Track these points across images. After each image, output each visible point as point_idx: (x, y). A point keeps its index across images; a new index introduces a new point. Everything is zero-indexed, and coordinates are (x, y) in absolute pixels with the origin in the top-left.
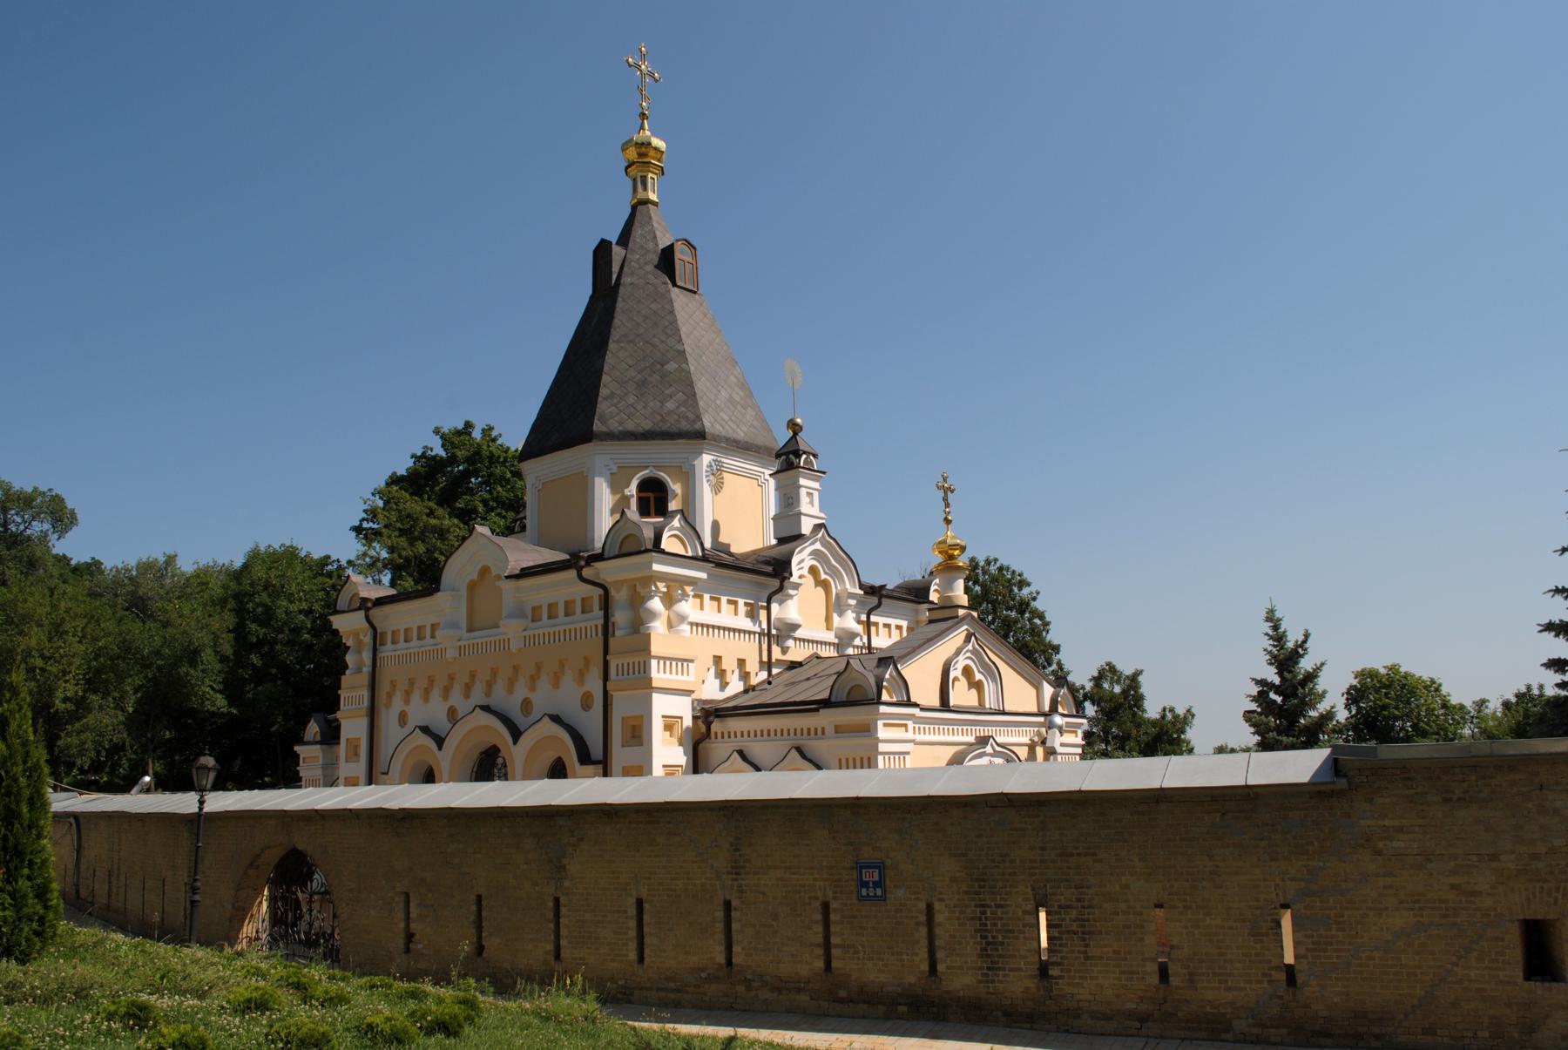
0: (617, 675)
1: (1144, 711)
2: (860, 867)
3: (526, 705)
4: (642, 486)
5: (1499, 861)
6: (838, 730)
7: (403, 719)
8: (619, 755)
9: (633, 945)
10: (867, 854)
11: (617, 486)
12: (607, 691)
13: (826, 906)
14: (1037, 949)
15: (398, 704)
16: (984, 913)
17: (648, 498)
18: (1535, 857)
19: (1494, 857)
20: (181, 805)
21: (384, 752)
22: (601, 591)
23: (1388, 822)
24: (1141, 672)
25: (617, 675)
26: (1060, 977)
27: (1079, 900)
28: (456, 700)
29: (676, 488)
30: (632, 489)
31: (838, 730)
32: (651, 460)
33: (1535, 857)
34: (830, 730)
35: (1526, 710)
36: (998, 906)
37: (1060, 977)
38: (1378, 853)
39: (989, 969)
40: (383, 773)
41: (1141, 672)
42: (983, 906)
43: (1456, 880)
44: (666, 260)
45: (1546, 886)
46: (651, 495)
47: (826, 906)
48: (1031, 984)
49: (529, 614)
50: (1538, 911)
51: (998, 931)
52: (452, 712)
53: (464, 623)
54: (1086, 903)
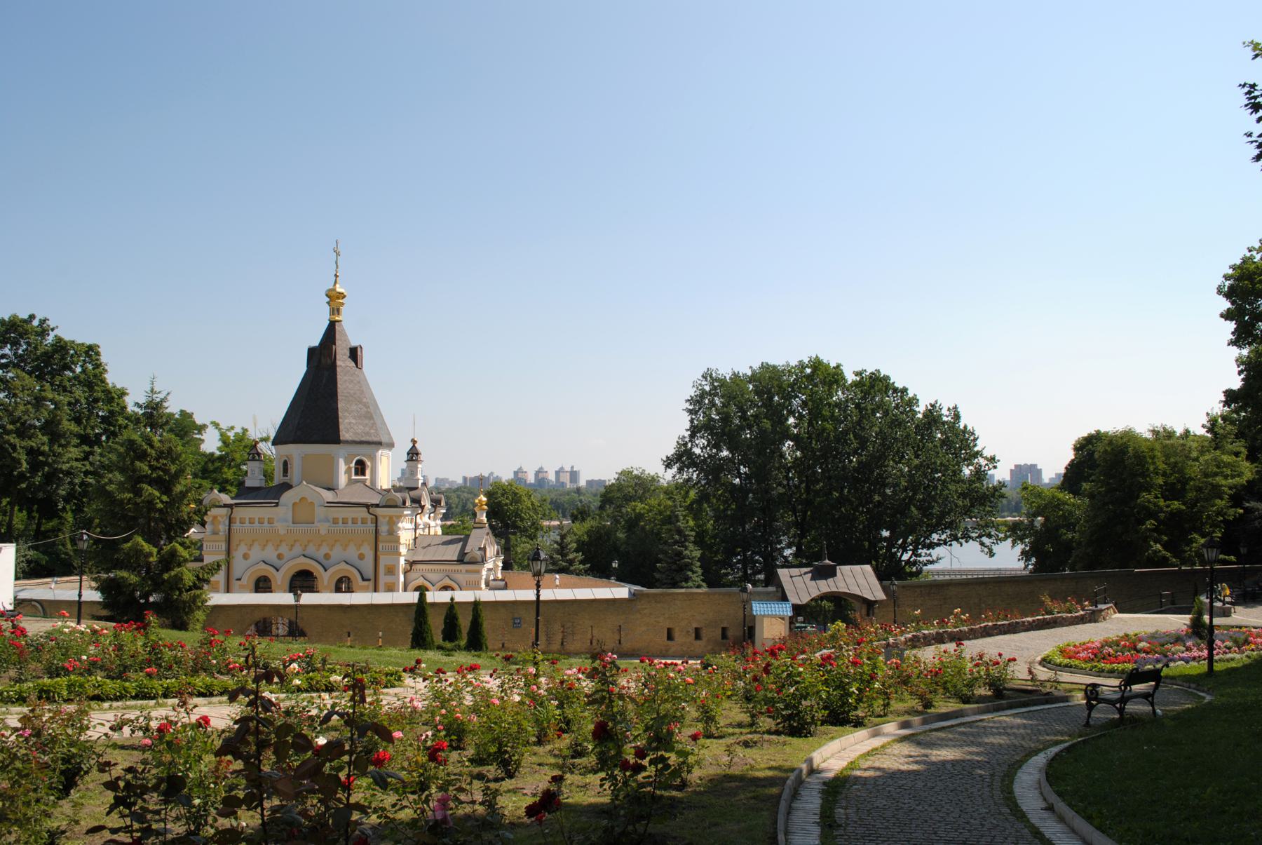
1: (108, 384)
2: (514, 619)
3: (327, 556)
4: (356, 464)
5: (934, 706)
6: (467, 571)
7: (246, 557)
8: (383, 579)
10: (516, 616)
11: (347, 462)
15: (242, 549)
21: (236, 572)
22: (374, 517)
28: (284, 549)
29: (368, 463)
30: (353, 465)
31: (467, 571)
32: (361, 453)
34: (464, 571)
40: (238, 580)
44: (354, 354)
46: (359, 467)
48: (559, 647)
49: (331, 520)
50: (671, 627)
52: (280, 557)
53: (291, 519)
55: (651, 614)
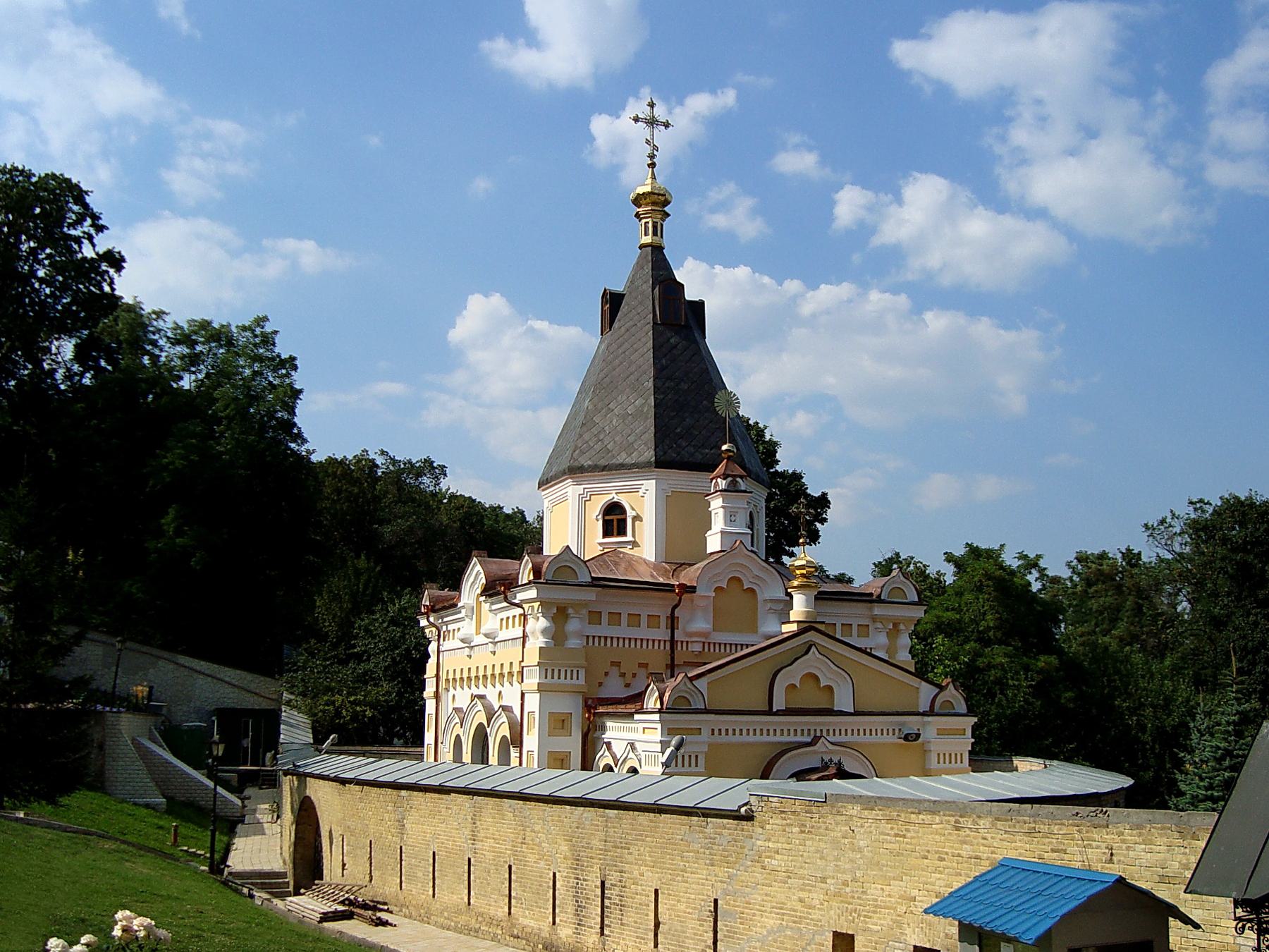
0: (939, 763)
9: (431, 889)
12: (1186, 923)
13: (510, 867)
14: (984, 942)
16: (577, 884)
17: (612, 520)
18: (845, 884)
19: (823, 880)
20: (1047, 903)
23: (771, 845)
24: (107, 228)
25: (939, 763)
26: (609, 936)
27: (620, 881)
33: (845, 884)
35: (55, 371)
36: (585, 880)
37: (609, 936)
38: (764, 868)
39: (579, 924)
41: (107, 228)
42: (577, 879)
43: (803, 895)
45: (850, 907)
47: (510, 867)
51: (584, 898)
54: (623, 884)
55: (789, 874)
